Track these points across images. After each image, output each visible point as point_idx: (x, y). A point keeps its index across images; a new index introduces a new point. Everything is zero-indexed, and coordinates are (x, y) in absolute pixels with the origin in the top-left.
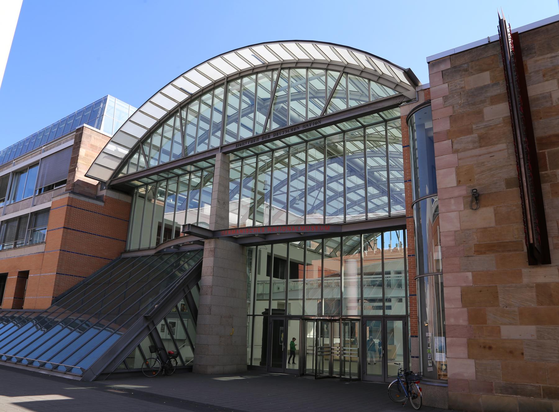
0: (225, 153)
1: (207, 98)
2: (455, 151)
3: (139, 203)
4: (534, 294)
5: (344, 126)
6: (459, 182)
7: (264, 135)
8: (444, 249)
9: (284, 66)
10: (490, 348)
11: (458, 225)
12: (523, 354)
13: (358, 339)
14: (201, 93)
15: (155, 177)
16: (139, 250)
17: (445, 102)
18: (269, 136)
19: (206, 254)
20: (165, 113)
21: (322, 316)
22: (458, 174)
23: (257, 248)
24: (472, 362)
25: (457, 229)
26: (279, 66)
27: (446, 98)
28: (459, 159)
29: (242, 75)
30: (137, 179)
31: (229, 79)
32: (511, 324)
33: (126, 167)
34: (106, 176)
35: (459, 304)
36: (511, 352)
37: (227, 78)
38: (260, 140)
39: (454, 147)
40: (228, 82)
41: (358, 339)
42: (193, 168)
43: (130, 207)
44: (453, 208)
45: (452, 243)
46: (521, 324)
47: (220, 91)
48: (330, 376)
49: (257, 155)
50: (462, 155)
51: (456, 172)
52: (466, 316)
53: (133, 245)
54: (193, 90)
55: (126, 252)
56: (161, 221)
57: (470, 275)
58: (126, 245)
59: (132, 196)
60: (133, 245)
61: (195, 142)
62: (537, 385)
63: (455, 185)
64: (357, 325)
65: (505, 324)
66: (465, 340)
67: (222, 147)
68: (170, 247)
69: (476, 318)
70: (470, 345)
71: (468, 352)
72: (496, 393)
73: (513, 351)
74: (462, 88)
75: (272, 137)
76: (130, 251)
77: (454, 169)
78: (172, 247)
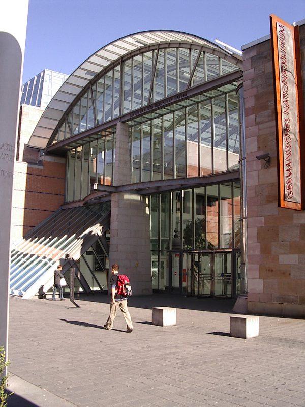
0: (123, 122)
1: (110, 74)
2: (257, 124)
3: (71, 161)
4: (299, 231)
5: (225, 88)
6: (259, 147)
7: (149, 107)
8: (248, 199)
9: (161, 47)
10: (272, 271)
11: (257, 181)
12: (290, 274)
13: (239, 268)
14: (104, 72)
15: (87, 139)
16: (73, 202)
17: (252, 84)
18: (145, 110)
19: (113, 204)
20: (81, 89)
21: (206, 250)
22: (258, 143)
23: (193, 191)
24: (261, 281)
25: (256, 184)
26: (157, 47)
27: (253, 80)
28: (259, 130)
29: (132, 55)
30: (68, 145)
31: (124, 59)
32: (285, 254)
33: (57, 136)
34: (43, 144)
35: (256, 240)
36: (284, 273)
37: (122, 58)
38: (174, 100)
39: (257, 119)
40: (123, 61)
41: (239, 268)
42: (143, 119)
43: (64, 167)
44: (255, 168)
45: (253, 195)
46: (290, 254)
47: (118, 68)
48: (191, 294)
49: (173, 112)
50: (261, 126)
51: (257, 140)
52: (259, 250)
53: (69, 199)
54: (98, 70)
55: (65, 204)
56: (94, 176)
57: (263, 218)
58: (64, 199)
59: (66, 158)
60: (69, 199)
61: (112, 108)
62: (296, 295)
63: (256, 150)
64: (229, 257)
65: (282, 254)
66: (257, 266)
67: (121, 117)
68: (91, 199)
69: (266, 250)
70: (261, 269)
71: (260, 273)
72: (274, 301)
73: (285, 273)
74: (263, 72)
75: (154, 108)
76: (68, 203)
77: (256, 138)
78: (93, 200)
